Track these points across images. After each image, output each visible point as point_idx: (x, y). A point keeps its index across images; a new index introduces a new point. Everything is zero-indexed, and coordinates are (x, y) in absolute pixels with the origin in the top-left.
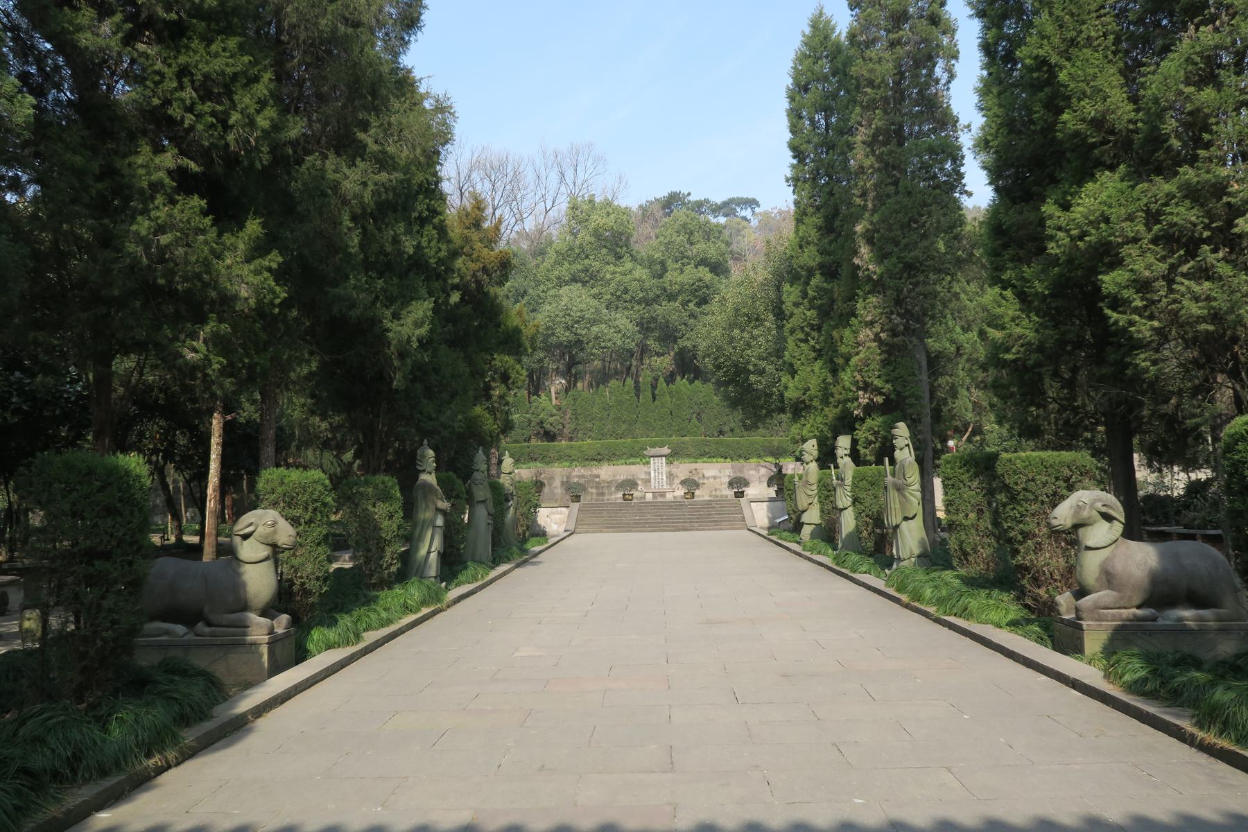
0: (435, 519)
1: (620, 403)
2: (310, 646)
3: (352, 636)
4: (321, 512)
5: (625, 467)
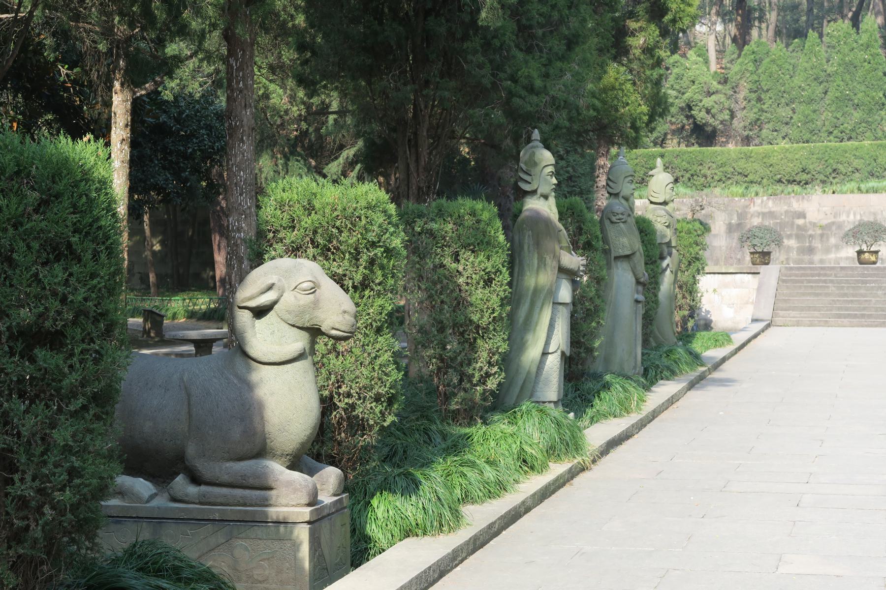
0: (558, 288)
1: (849, 67)
2: (373, 529)
3: (447, 514)
4: (382, 267)
5: (857, 196)
